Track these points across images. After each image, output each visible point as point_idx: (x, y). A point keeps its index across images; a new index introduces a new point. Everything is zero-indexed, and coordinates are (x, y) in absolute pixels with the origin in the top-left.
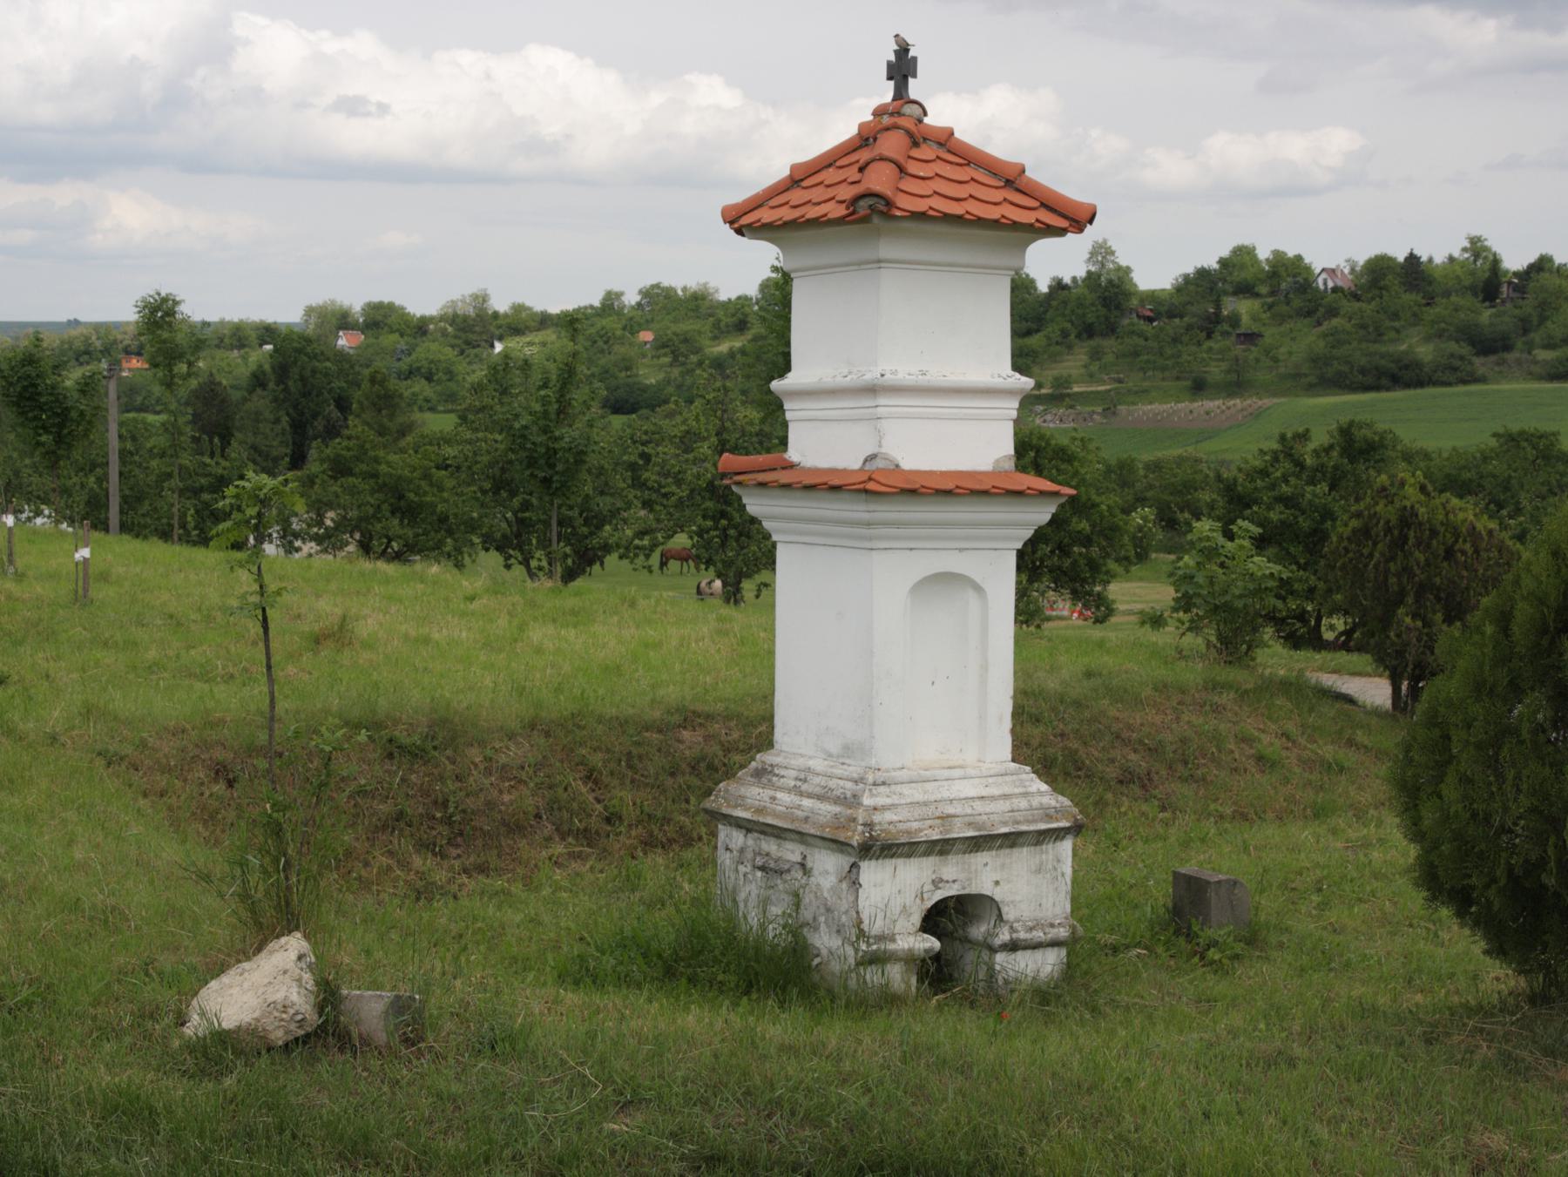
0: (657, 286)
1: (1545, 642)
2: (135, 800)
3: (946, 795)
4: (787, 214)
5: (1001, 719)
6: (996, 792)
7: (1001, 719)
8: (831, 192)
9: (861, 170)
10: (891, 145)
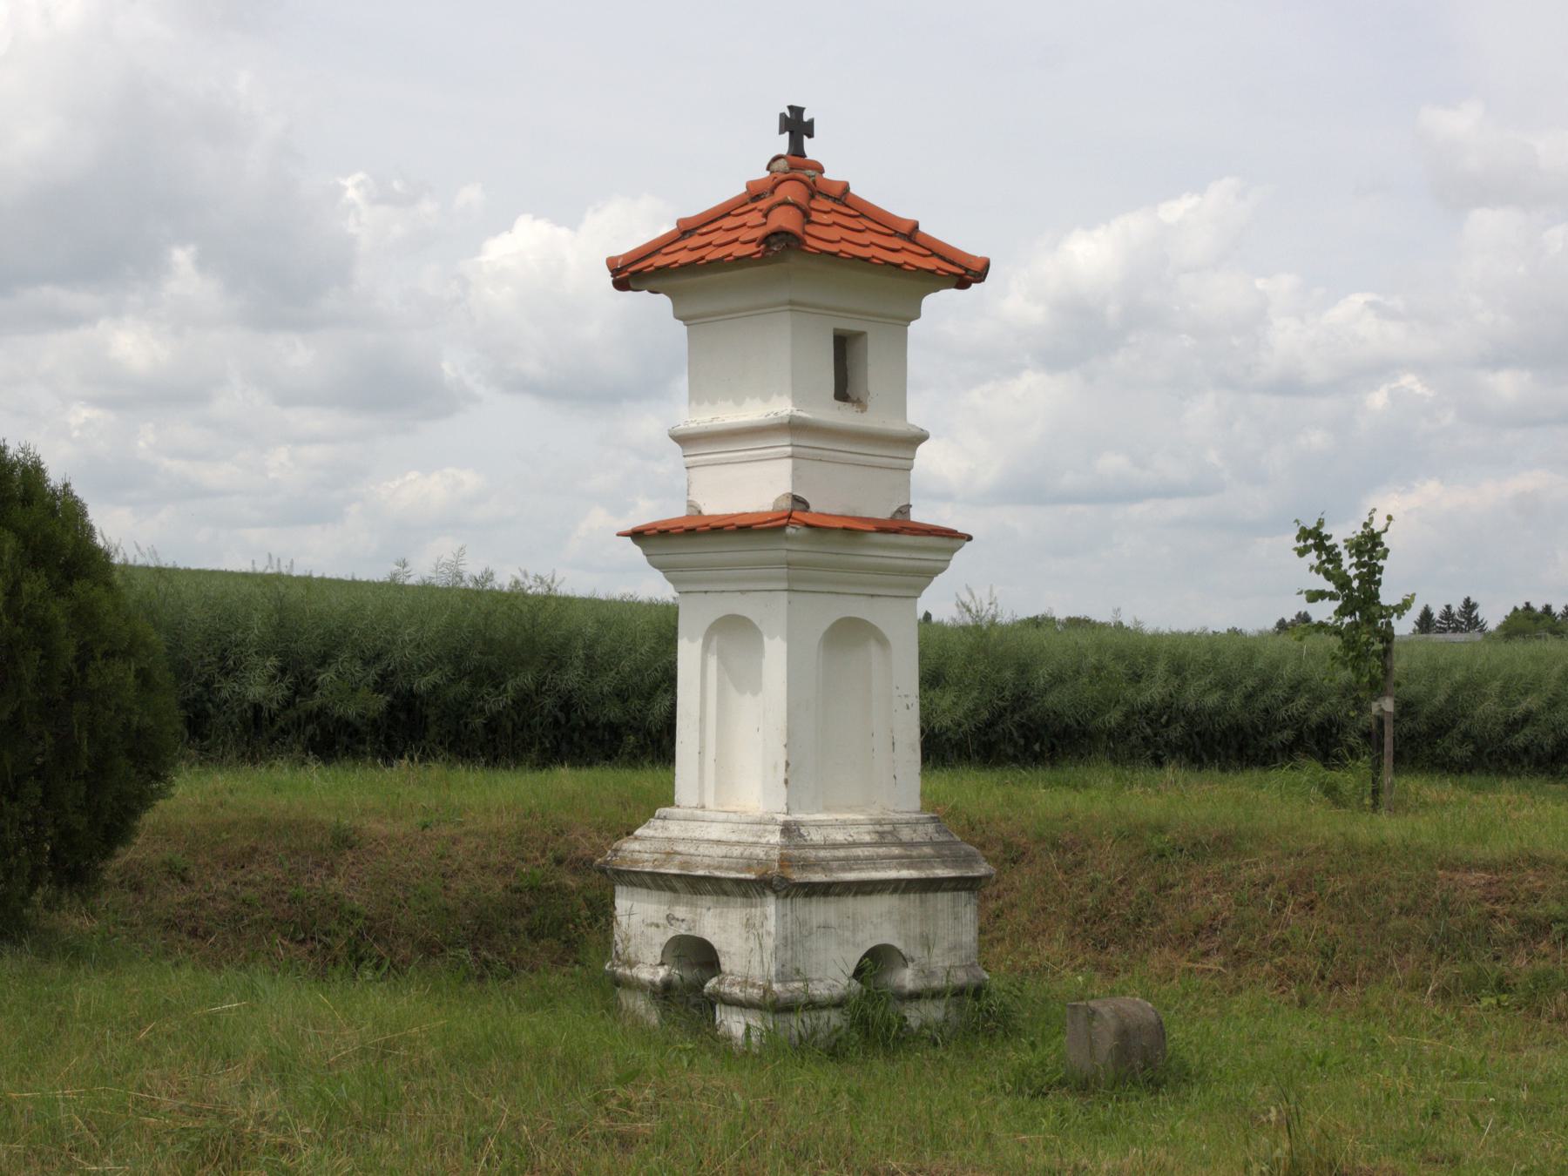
0: (83, 507)
1: (258, 687)
2: (1293, 935)
3: (697, 834)
4: (684, 257)
5: (775, 767)
6: (734, 838)
7: (775, 767)
8: (733, 235)
9: (766, 216)
10: (789, 191)
